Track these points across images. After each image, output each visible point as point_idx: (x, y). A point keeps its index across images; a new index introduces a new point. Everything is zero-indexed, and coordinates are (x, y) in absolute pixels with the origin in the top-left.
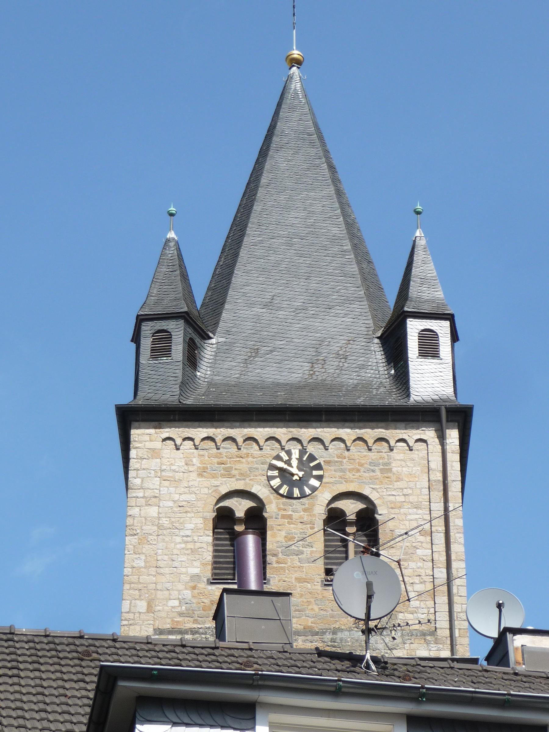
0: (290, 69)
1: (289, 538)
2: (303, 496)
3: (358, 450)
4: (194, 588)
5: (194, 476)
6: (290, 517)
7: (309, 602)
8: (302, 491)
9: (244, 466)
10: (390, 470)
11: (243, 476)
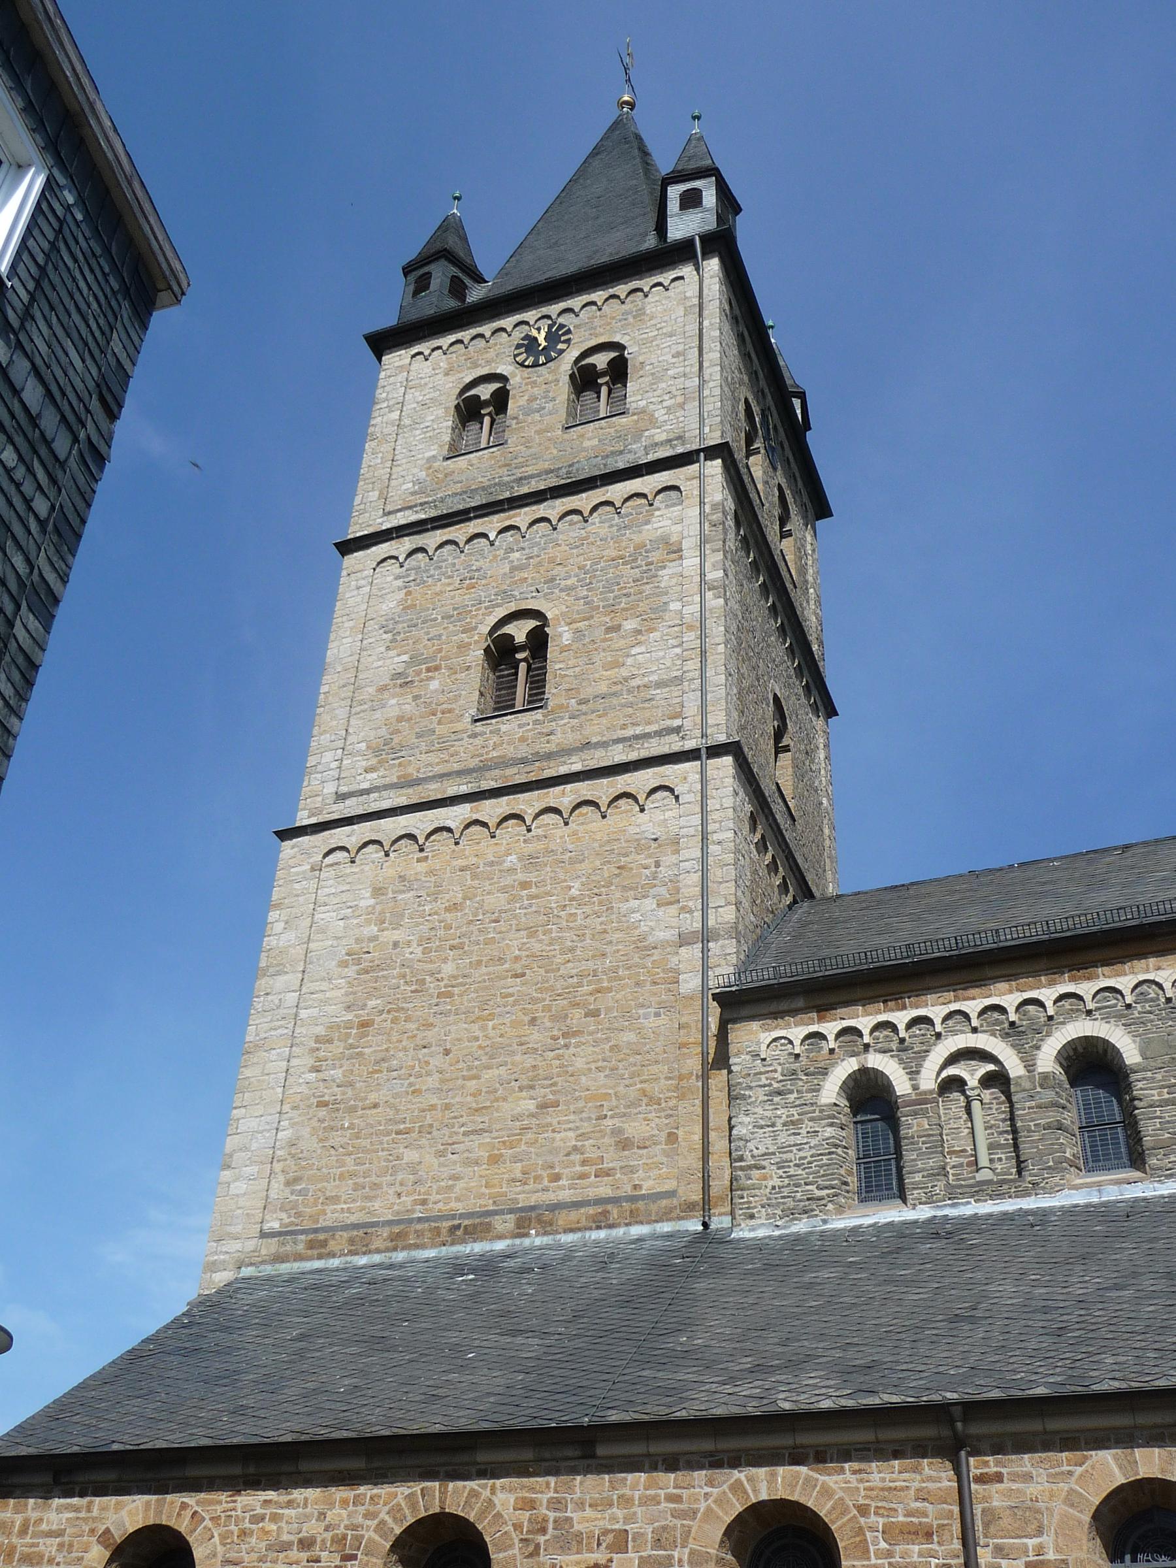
0: (382, 343)
3: (613, 307)
4: (430, 468)
6: (535, 382)
7: (547, 449)
9: (491, 354)
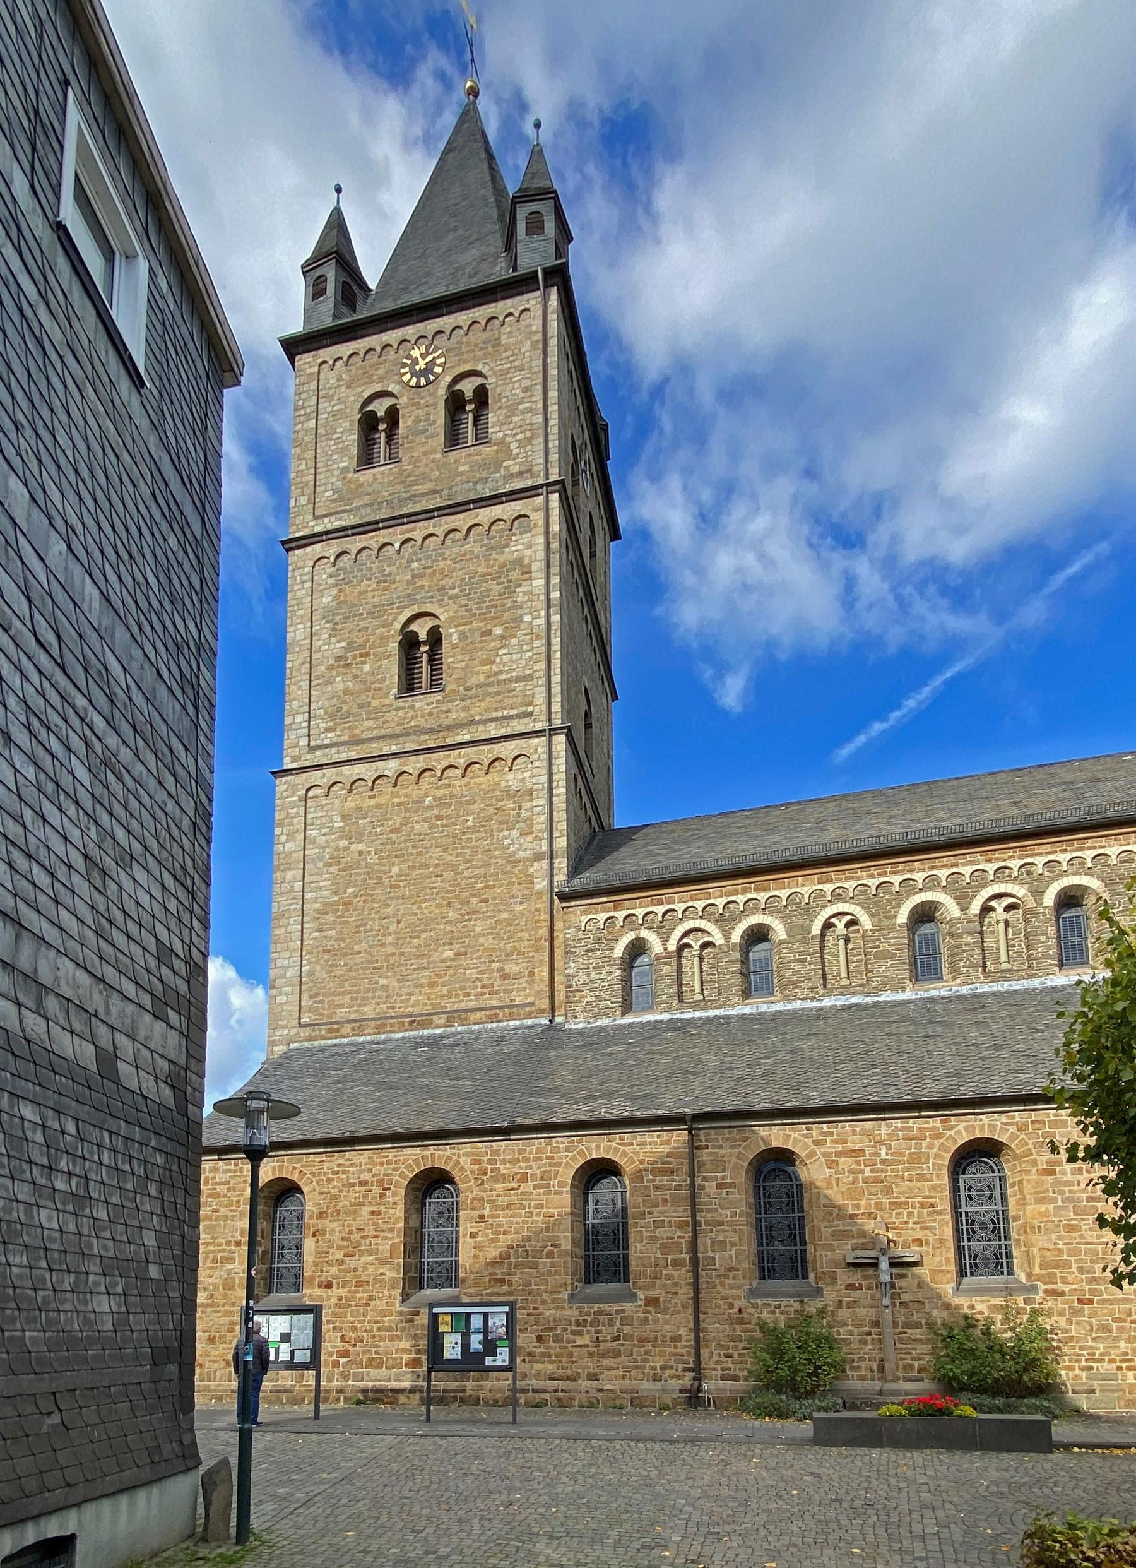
1: (418, 420)
2: (429, 383)
4: (344, 478)
5: (343, 389)
8: (427, 379)
10: (500, 344)
11: (381, 379)
